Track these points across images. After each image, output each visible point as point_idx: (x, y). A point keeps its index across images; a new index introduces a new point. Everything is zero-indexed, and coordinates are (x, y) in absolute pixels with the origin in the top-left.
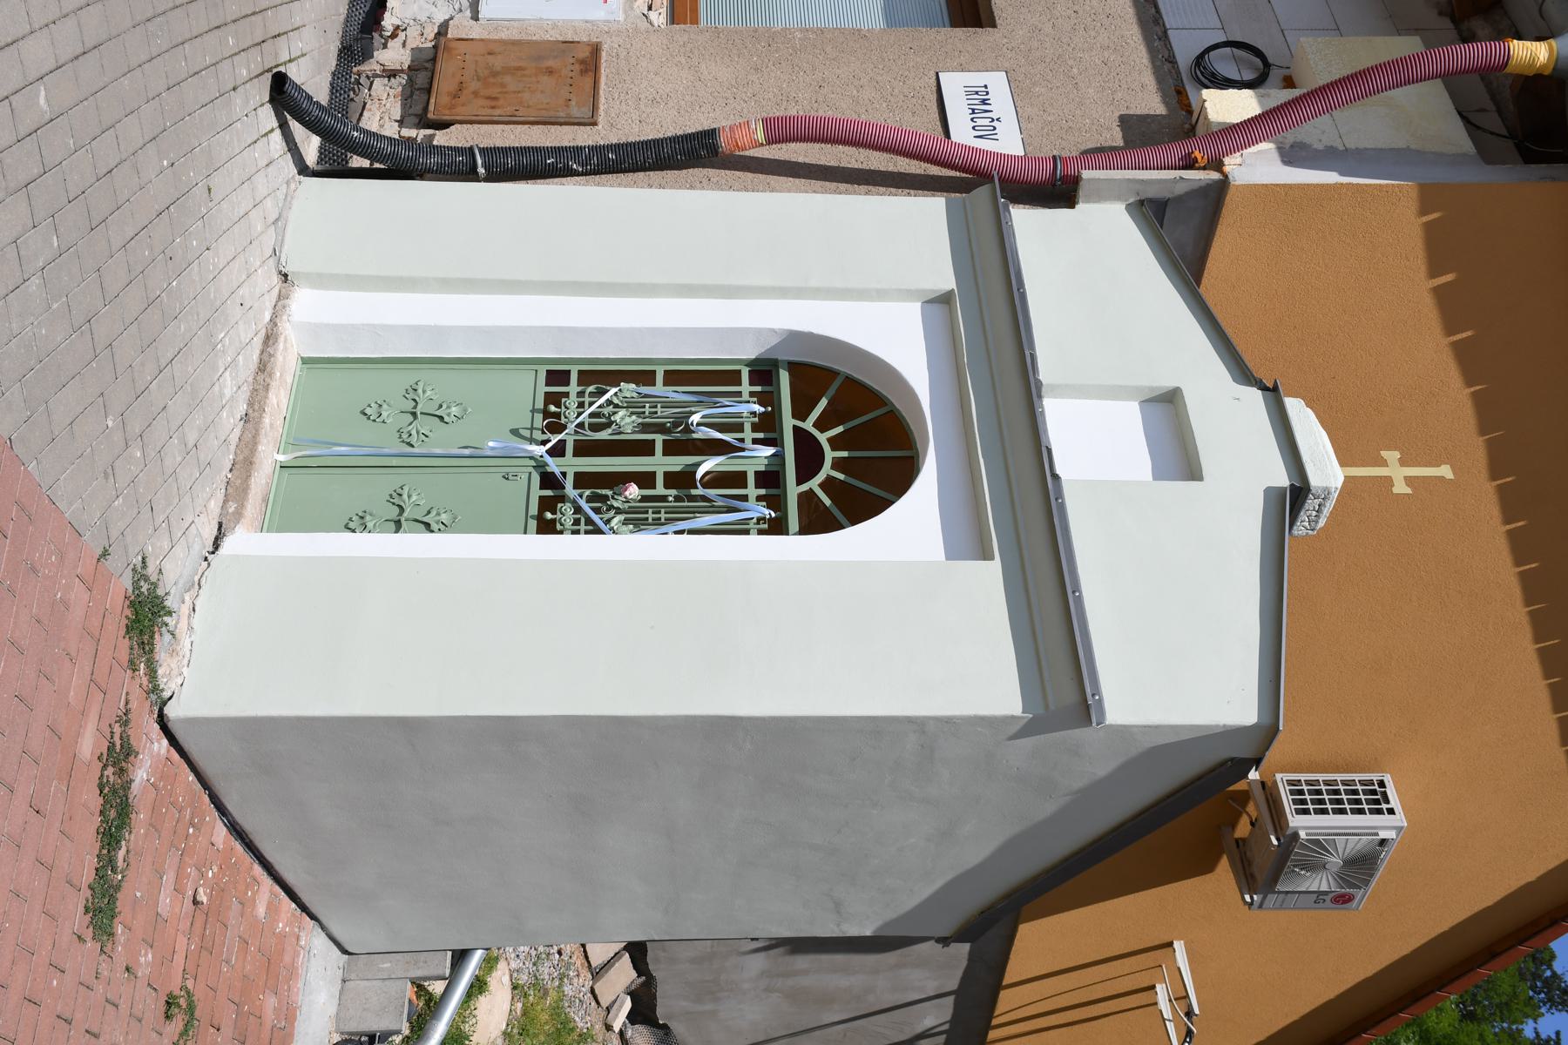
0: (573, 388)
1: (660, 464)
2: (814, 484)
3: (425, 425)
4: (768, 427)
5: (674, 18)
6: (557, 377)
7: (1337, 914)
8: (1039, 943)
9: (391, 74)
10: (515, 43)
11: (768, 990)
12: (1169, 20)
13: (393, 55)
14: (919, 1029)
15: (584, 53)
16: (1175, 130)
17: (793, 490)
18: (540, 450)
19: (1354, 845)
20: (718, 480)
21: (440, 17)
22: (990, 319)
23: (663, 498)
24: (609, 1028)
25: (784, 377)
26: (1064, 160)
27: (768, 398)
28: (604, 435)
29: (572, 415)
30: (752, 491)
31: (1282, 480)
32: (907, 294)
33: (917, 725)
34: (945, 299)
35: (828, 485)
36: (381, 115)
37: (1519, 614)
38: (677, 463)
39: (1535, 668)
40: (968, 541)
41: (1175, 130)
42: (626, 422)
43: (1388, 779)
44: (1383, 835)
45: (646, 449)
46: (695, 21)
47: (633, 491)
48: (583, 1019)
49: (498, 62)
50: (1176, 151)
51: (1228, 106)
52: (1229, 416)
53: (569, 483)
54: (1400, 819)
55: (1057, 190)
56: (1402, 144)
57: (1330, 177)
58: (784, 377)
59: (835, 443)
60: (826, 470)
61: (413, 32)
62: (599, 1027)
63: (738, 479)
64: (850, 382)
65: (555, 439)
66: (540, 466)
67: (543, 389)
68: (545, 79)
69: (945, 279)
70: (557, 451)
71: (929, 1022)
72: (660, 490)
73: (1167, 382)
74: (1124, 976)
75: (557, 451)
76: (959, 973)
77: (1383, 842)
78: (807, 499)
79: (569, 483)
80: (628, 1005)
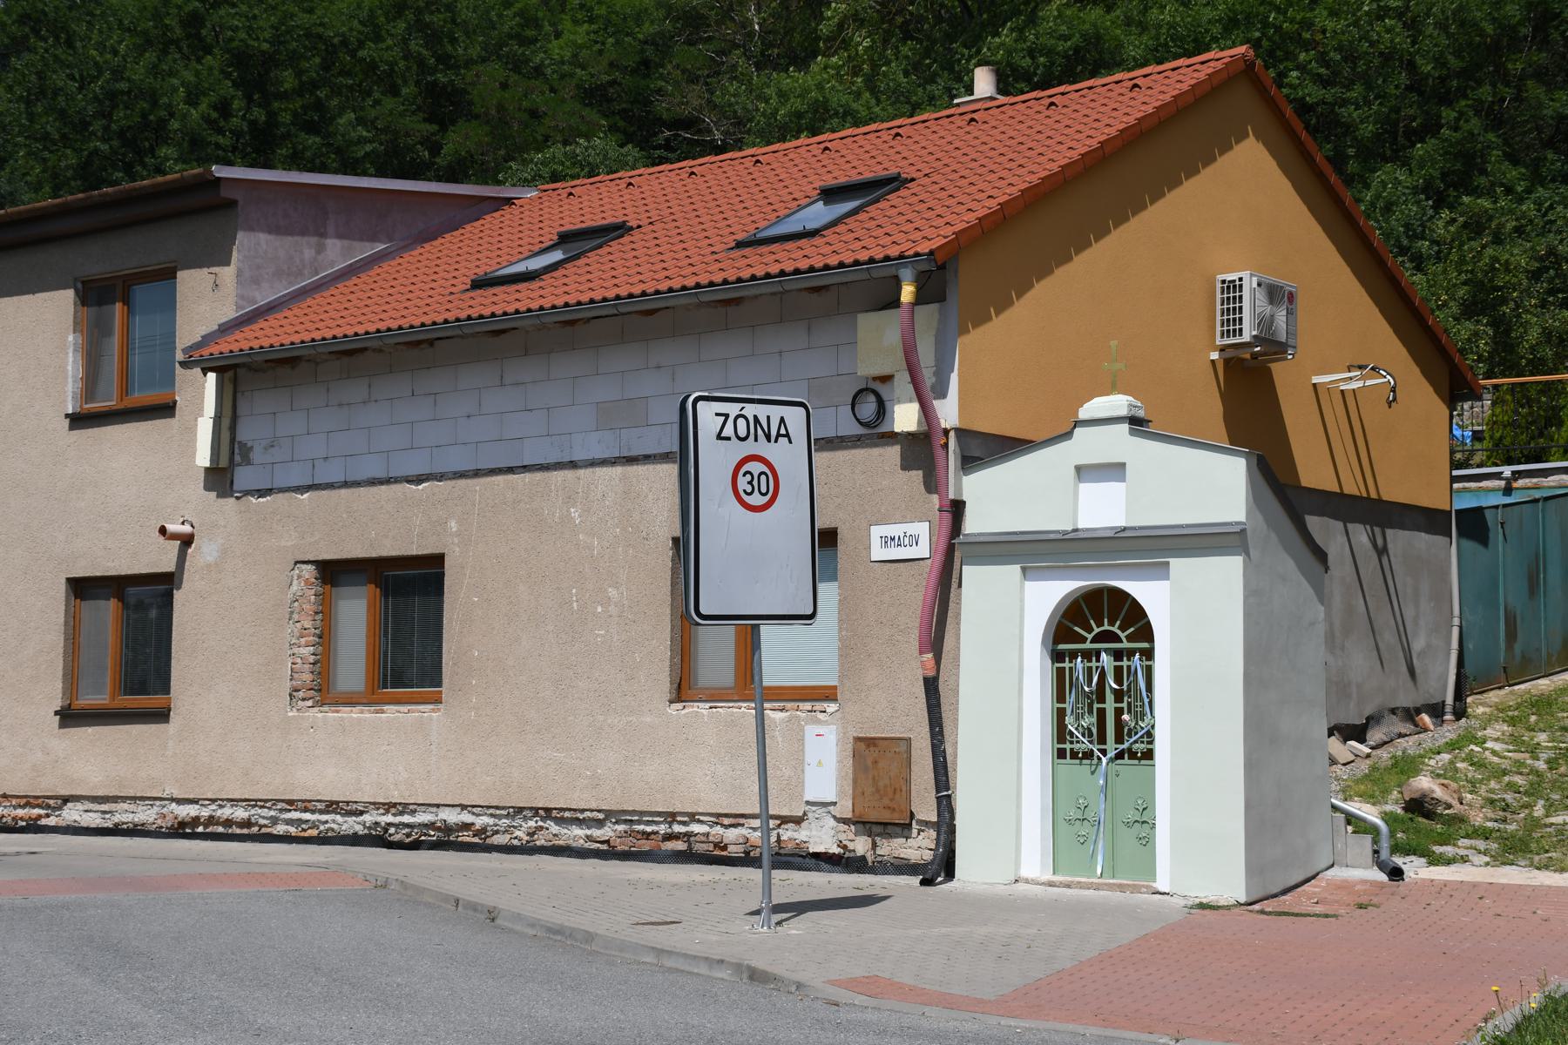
0: (1068, 746)
1: (1110, 705)
2: (1122, 635)
3: (1090, 814)
4: (1087, 655)
5: (835, 700)
6: (1061, 754)
7: (1300, 301)
8: (1314, 473)
9: (874, 846)
10: (855, 781)
11: (1343, 648)
12: (832, 434)
13: (861, 846)
14: (1369, 545)
15: (862, 746)
16: (920, 450)
17: (1125, 645)
18: (1104, 760)
19: (1261, 296)
20: (1118, 680)
21: (832, 823)
22: (1031, 551)
23: (1129, 704)
24: (1368, 756)
25: (1061, 647)
26: (941, 506)
27: (1073, 655)
28: (1094, 730)
29: (1085, 745)
30: (1125, 663)
31: (1126, 427)
32: (1022, 588)
33: (1246, 598)
34: (1024, 569)
35: (1122, 629)
36: (919, 847)
37: (1135, 222)
38: (1110, 697)
39: (1161, 204)
40: (1162, 571)
41: (920, 450)
42: (1089, 721)
43: (1220, 277)
44: (1255, 285)
45: (1102, 714)
46: (835, 688)
47: (1126, 717)
48: (1364, 767)
49: (869, 790)
50: (939, 452)
51: (905, 417)
52: (1087, 445)
53: (1121, 747)
54: (1245, 274)
55: (957, 509)
56: (933, 339)
57: (954, 378)
58: (1061, 647)
59: (1100, 624)
60: (1115, 629)
61: (842, 837)
62: (1367, 762)
63: (1118, 672)
64: (1065, 615)
65: (1097, 753)
66: (1111, 760)
67: (1068, 760)
68: (880, 765)
69: (1017, 568)
70: (1104, 752)
71: (1364, 539)
72: (1125, 705)
73: (1073, 470)
74: (1334, 415)
75: (1104, 752)
76: (1332, 521)
77: (1259, 285)
78: (1130, 638)
79: (1121, 747)
80: (1353, 743)
